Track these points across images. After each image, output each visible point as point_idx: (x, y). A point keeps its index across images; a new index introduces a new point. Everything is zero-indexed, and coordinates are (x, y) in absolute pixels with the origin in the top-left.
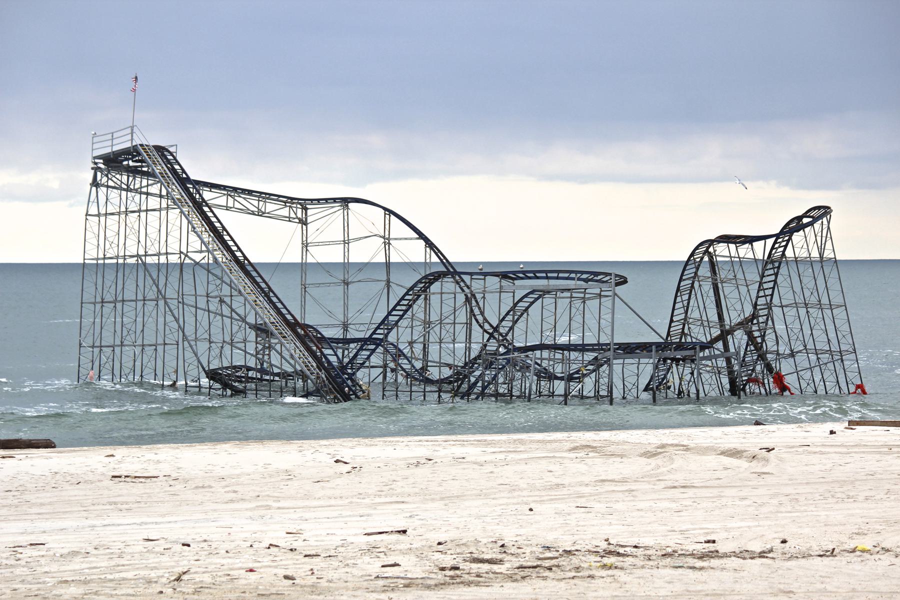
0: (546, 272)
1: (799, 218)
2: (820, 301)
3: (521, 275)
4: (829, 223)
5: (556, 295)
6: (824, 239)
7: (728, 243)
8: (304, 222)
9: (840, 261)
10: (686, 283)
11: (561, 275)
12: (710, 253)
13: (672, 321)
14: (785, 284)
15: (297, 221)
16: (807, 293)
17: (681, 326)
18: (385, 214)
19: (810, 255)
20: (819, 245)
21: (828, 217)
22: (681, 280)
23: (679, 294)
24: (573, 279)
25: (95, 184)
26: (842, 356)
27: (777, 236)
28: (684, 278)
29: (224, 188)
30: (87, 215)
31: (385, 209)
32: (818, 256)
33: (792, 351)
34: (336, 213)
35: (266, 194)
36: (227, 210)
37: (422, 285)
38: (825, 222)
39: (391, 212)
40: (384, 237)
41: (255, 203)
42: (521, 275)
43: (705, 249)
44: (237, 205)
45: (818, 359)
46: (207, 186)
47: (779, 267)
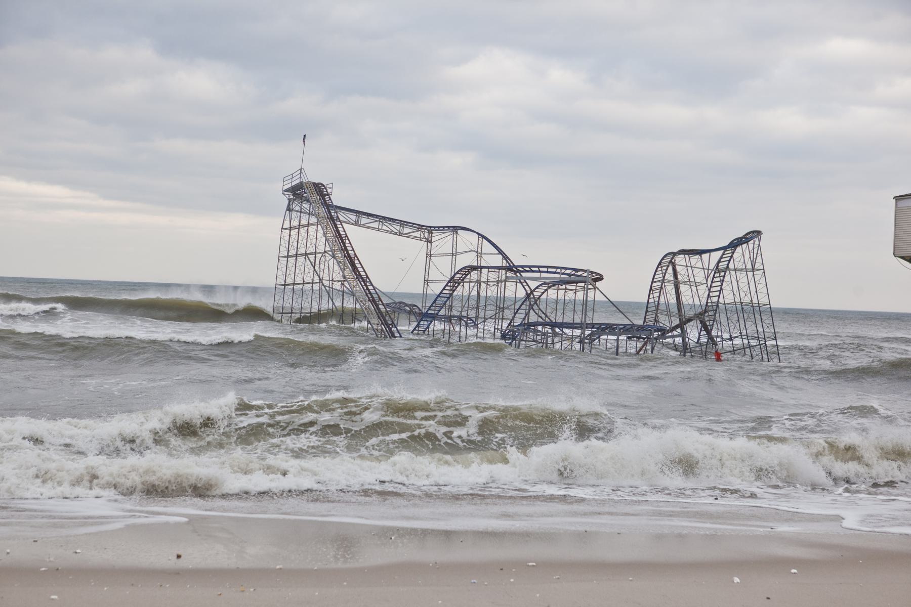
0: (539, 267)
1: (741, 238)
2: (752, 301)
3: (527, 269)
4: (759, 241)
5: (558, 287)
6: (755, 255)
7: (685, 254)
8: (429, 241)
9: (774, 308)
10: (657, 285)
11: (550, 270)
12: (673, 263)
13: (647, 311)
14: (727, 288)
15: (425, 240)
16: (742, 295)
17: (654, 316)
18: (479, 237)
19: (746, 267)
20: (752, 259)
21: (759, 237)
22: (653, 282)
23: (651, 293)
24: (558, 273)
25: (289, 209)
26: (765, 341)
27: (724, 248)
28: (655, 280)
29: (377, 216)
30: (282, 228)
31: (479, 234)
32: (751, 268)
33: (731, 336)
34: (448, 237)
35: (404, 222)
36: (378, 230)
37: (460, 276)
38: (757, 242)
39: (484, 237)
40: (477, 252)
41: (398, 228)
42: (527, 269)
43: (670, 260)
44: (384, 228)
45: (749, 342)
46: (365, 215)
47: (724, 276)
